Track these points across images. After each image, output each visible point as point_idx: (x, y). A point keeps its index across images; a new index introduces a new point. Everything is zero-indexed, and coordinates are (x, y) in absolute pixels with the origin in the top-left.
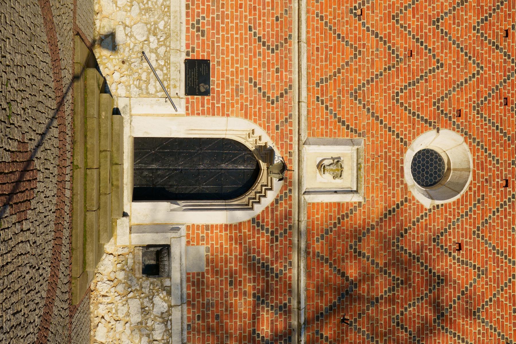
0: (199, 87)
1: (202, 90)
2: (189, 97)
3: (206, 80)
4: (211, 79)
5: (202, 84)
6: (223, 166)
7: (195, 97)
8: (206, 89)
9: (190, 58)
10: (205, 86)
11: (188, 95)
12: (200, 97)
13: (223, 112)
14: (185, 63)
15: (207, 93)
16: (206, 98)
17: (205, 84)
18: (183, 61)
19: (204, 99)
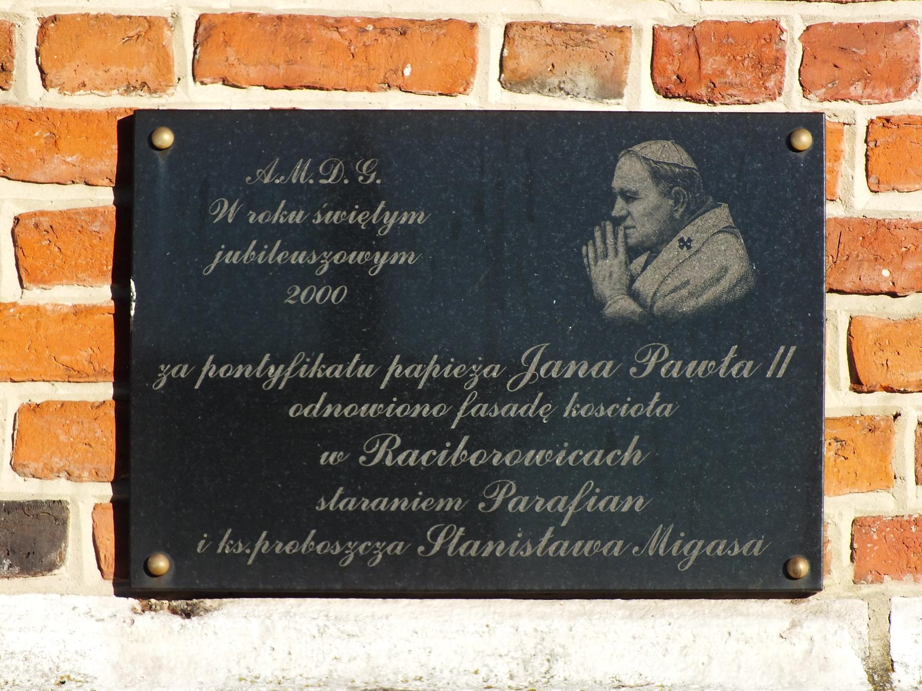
0: (655, 326)
1: (711, 261)
2: (840, 511)
3: (525, 181)
4: (487, 94)
5: (606, 272)
6: (132, 313)
7: (838, 399)
8: (689, 193)
9: (88, 501)
10: (644, 211)
11: (811, 544)
12: (838, 310)
13: (110, 113)
14: (190, 590)
15: (762, 174)
16: (851, 196)
17: (597, 203)
18: (159, 629)
19: (877, 234)
